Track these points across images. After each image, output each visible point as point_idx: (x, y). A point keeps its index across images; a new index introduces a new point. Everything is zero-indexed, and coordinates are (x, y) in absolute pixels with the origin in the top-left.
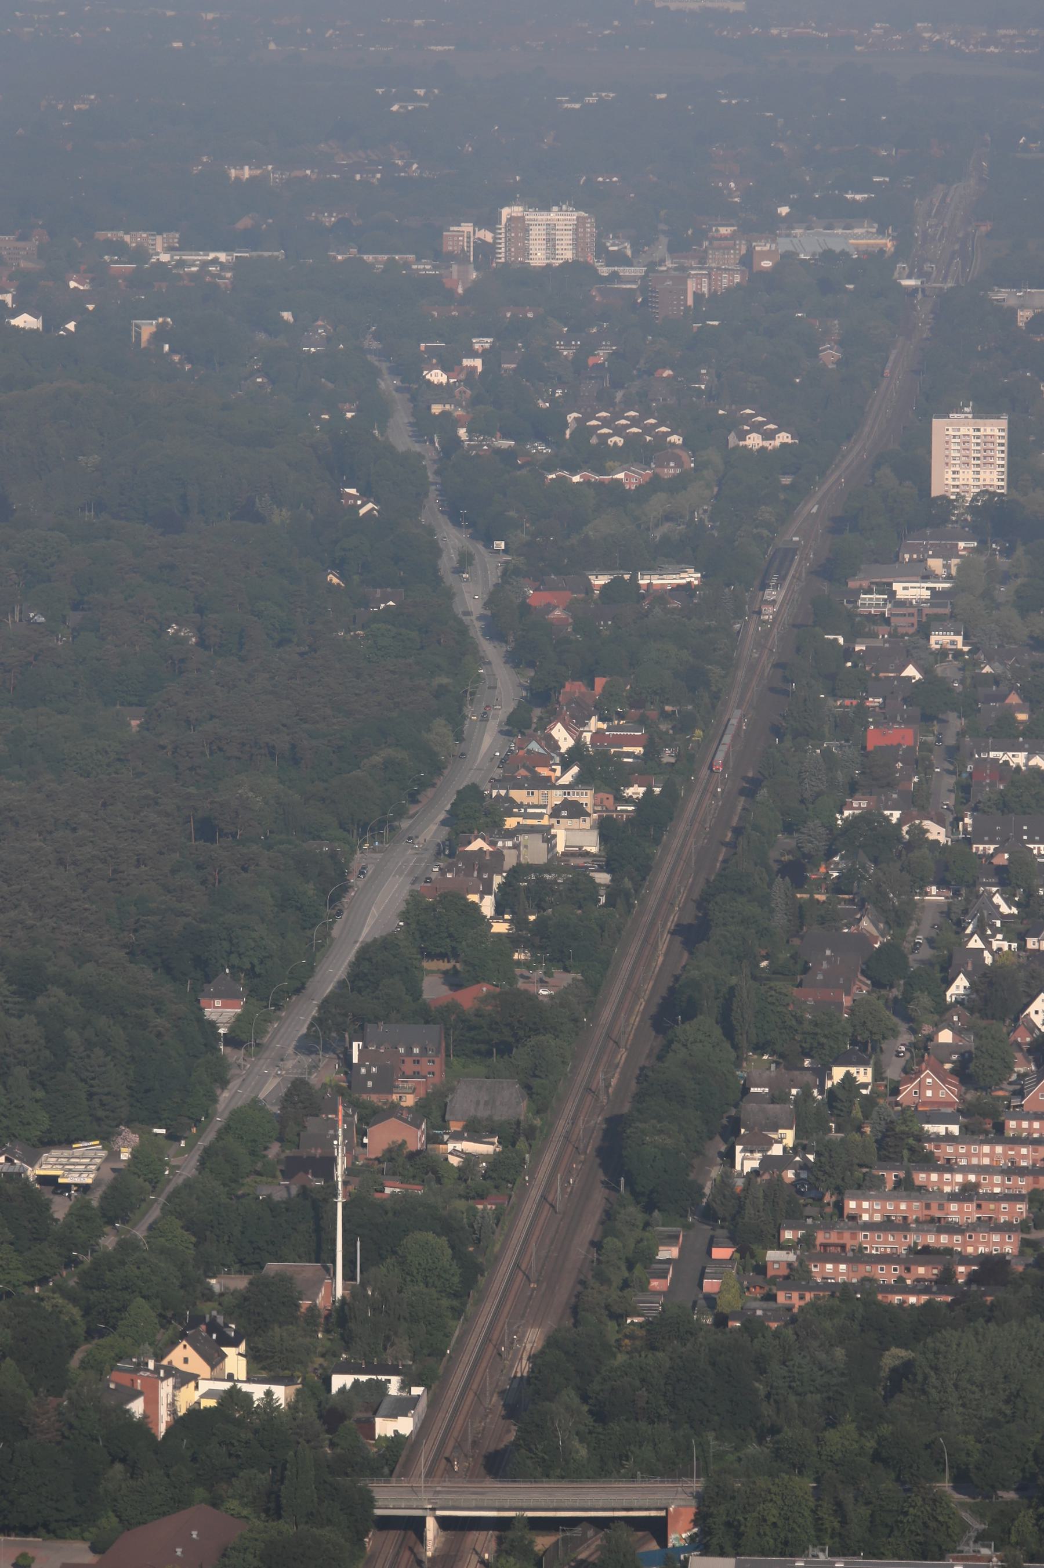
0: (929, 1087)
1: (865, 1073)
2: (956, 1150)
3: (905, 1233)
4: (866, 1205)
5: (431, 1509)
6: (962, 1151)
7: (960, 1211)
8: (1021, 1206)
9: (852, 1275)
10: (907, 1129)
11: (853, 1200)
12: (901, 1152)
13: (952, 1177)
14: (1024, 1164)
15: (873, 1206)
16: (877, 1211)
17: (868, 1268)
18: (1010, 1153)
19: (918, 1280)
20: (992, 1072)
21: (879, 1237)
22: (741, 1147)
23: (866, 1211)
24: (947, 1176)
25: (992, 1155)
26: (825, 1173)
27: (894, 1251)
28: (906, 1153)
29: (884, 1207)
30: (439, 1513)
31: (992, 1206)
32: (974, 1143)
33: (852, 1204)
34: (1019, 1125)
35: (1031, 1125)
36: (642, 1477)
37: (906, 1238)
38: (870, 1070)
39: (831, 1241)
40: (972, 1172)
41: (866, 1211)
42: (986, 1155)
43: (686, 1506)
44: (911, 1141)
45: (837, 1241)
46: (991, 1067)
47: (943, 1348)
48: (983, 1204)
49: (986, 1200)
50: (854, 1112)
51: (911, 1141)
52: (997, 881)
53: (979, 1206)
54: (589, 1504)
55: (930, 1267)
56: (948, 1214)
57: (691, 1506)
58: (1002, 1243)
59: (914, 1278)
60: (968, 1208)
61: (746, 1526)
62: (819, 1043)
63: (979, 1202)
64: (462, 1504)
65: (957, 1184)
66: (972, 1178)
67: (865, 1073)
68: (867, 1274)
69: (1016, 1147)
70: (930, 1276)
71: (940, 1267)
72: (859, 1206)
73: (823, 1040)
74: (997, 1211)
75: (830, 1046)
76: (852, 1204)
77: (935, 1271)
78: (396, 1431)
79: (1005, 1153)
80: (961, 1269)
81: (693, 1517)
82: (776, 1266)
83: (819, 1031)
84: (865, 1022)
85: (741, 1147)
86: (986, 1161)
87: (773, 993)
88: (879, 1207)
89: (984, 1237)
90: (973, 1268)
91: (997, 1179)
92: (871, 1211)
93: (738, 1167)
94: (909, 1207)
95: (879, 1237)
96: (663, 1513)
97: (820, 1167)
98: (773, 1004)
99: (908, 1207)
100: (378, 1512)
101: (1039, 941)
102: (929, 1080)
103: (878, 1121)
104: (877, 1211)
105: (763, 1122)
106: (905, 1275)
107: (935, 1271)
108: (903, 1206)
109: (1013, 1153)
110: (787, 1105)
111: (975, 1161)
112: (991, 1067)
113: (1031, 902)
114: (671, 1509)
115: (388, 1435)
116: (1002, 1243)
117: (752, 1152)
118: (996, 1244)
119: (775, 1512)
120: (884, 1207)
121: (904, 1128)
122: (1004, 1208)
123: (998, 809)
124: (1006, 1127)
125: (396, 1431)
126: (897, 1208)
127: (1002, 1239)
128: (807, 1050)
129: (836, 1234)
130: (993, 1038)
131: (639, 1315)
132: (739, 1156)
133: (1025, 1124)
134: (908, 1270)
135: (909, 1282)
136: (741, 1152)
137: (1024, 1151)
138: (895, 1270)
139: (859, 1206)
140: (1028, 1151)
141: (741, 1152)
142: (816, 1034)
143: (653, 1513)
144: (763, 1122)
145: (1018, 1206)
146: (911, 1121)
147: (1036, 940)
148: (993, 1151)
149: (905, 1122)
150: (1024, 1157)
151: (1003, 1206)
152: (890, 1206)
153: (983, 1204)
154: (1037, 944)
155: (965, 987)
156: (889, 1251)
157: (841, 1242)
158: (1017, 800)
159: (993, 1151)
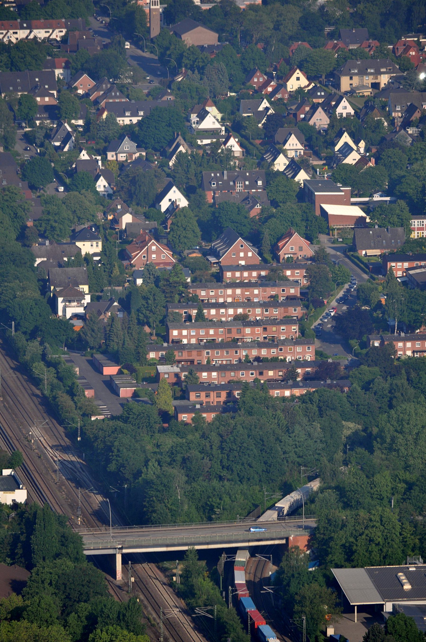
0: (154, 252)
1: (97, 246)
2: (208, 293)
3: (236, 349)
4: (185, 332)
5: (120, 549)
6: (212, 294)
7: (253, 333)
8: (294, 328)
9: (221, 379)
10: (179, 279)
11: (176, 330)
12: (174, 296)
13: (226, 311)
14: (256, 300)
15: (190, 333)
16: (193, 337)
17: (233, 374)
18: (246, 293)
19: (269, 380)
20: (186, 240)
21: (217, 353)
22: (62, 298)
23: (185, 337)
24: (222, 311)
25: (233, 296)
26: (151, 311)
27: (229, 362)
28: (177, 297)
29: (198, 334)
30: (125, 551)
31: (274, 329)
32: (220, 287)
33: (175, 333)
34: (233, 275)
35: (242, 275)
36: (240, 519)
37: (236, 352)
38: (100, 243)
39: (183, 358)
40: (240, 307)
41: (185, 337)
42: (229, 296)
43: (301, 535)
44: (181, 288)
45: (187, 358)
46: (185, 237)
47: (406, 417)
48: (268, 327)
49: (269, 324)
50: (115, 272)
51: (181, 288)
52: (48, 116)
53: (265, 329)
54: (234, 538)
55: (277, 371)
56: (244, 336)
57: (305, 535)
58: (304, 353)
59: (266, 379)
60: (258, 331)
61: (357, 545)
62: (52, 227)
63: (265, 326)
64: (143, 543)
65: (230, 316)
66: (240, 311)
67: (97, 246)
68: (232, 379)
69: (251, 289)
70: (277, 377)
71: (284, 371)
72: (180, 334)
73: (54, 224)
74: (278, 331)
75: (60, 228)
76: (175, 333)
77: (281, 373)
78: (14, 501)
79: (243, 293)
80: (299, 371)
81: (307, 543)
82: (166, 376)
83: (50, 217)
84: (75, 211)
85: (62, 298)
86: (229, 300)
87: (7, 193)
88: (194, 334)
89: (291, 349)
90: (307, 369)
91: (258, 311)
92: (189, 337)
93: (60, 313)
94: (216, 333)
95: (217, 353)
96: (284, 542)
97: (147, 307)
98: (7, 200)
99: (214, 332)
100: (87, 553)
101: (116, 155)
102: (154, 248)
103: (148, 276)
104: (193, 337)
105: (67, 281)
106: (259, 377)
107: (281, 373)
108: (212, 332)
109: (248, 293)
110: (81, 268)
111: (221, 300)
112: (185, 237)
113: (91, 128)
114: (291, 538)
115: (8, 504)
116: (304, 351)
117: (70, 302)
118: (299, 353)
119: (380, 534)
120: (198, 334)
121: (176, 279)
122: (283, 330)
123: (7, 68)
124: (224, 277)
125: (14, 501)
126: (207, 333)
127: (304, 350)
128: (42, 232)
129: (186, 353)
130: (185, 216)
131: (100, 414)
132: (60, 306)
133: (238, 274)
134: (261, 374)
135: (262, 382)
136: (62, 302)
137: (256, 292)
138: (252, 374)
139: (180, 334)
140: (259, 291)
141: (62, 302)
142: (49, 220)
143: (277, 542)
144: (67, 281)
145: (293, 328)
146: (181, 274)
147: (114, 153)
148: (234, 293)
149: (176, 274)
150: (257, 296)
151: (282, 328)
152: (202, 332)
153: (268, 327)
154: (115, 157)
155: (104, 186)
156: (224, 362)
157: (191, 358)
158: (22, 60)
159: (234, 293)
